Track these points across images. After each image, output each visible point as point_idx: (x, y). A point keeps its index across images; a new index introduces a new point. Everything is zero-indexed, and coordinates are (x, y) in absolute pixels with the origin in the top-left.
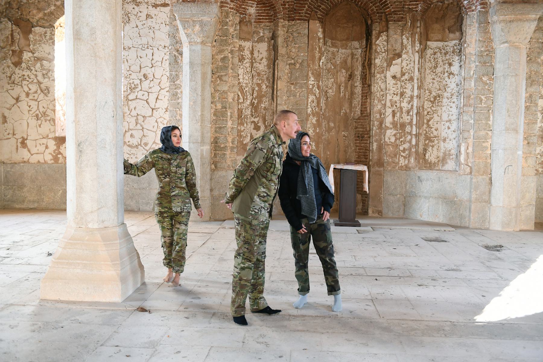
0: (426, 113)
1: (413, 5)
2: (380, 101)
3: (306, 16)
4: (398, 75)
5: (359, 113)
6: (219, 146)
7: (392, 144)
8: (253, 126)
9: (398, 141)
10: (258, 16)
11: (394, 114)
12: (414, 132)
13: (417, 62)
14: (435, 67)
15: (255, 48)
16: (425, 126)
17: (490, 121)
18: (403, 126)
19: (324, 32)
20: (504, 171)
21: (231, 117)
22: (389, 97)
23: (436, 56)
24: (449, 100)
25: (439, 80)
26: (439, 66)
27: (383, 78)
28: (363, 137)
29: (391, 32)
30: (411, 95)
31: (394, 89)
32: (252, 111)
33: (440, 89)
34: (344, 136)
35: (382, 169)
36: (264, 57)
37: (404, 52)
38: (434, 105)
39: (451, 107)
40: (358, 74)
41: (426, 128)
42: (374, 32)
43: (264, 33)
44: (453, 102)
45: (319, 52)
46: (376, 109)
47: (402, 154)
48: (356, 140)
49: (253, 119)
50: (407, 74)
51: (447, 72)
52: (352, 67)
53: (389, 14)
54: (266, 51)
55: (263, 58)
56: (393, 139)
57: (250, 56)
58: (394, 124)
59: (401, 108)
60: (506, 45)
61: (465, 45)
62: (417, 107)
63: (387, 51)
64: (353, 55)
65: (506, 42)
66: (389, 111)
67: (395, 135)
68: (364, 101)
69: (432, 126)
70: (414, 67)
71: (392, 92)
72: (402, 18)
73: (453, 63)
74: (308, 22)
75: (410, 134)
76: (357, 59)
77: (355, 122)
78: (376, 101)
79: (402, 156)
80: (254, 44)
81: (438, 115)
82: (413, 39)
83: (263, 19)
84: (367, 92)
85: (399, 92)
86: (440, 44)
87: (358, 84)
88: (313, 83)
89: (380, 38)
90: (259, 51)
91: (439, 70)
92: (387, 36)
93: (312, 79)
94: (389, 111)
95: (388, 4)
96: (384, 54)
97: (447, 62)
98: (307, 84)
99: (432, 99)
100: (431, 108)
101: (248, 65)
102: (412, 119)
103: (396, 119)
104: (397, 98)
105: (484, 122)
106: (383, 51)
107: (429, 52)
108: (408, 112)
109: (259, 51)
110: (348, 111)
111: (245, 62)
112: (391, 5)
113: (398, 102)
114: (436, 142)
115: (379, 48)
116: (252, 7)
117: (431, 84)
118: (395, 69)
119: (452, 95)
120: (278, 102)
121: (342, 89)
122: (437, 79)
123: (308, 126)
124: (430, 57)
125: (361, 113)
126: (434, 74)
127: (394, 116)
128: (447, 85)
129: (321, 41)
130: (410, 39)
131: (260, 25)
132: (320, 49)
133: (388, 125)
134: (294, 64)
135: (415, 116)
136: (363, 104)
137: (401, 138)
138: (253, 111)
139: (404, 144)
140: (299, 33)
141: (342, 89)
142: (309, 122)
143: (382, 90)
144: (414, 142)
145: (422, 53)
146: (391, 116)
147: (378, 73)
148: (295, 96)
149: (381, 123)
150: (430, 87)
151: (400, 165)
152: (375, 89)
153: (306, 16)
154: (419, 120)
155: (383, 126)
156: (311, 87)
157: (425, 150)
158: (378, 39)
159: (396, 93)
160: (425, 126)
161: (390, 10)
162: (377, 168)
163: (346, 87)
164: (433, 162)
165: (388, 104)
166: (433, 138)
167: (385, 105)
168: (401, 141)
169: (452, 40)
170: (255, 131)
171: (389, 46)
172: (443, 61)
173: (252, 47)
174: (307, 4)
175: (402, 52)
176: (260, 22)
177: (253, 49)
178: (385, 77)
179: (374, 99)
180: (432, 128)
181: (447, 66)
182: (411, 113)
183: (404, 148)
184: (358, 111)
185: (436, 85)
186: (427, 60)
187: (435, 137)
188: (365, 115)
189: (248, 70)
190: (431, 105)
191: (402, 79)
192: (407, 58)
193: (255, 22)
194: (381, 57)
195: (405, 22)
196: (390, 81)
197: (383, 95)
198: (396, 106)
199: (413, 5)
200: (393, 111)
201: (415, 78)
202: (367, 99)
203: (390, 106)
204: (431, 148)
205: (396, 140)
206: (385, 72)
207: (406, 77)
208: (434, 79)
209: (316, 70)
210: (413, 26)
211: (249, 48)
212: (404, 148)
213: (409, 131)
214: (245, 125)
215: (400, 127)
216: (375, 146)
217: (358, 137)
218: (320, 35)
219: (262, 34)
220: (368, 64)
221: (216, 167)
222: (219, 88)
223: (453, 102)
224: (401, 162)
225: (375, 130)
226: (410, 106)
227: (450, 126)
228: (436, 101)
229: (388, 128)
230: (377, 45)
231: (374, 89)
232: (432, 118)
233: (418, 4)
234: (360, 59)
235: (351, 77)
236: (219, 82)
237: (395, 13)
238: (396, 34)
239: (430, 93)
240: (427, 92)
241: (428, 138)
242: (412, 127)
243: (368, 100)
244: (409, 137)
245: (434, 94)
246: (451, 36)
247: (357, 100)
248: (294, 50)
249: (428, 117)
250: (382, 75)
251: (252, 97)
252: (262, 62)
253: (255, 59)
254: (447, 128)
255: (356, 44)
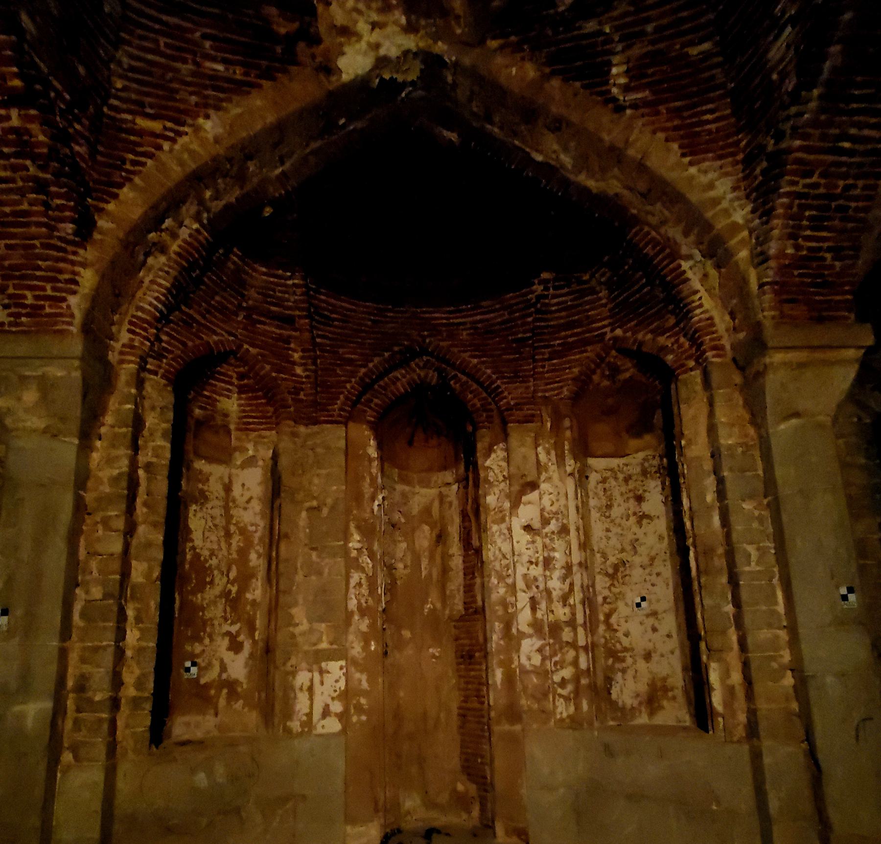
0: (600, 599)
1: (553, 389)
2: (501, 578)
3: (340, 416)
4: (536, 524)
5: (460, 607)
6: (90, 701)
7: (536, 671)
8: (226, 642)
9: (548, 662)
10: (245, 417)
11: (534, 604)
12: (582, 642)
13: (571, 494)
14: (609, 507)
15: (234, 480)
16: (602, 628)
17: (776, 603)
18: (555, 629)
19: (380, 447)
20: (853, 733)
21: (138, 620)
22: (521, 570)
23: (607, 485)
24: (647, 571)
25: (621, 532)
26: (615, 505)
27: (506, 531)
28: (471, 657)
29: (514, 441)
30: (567, 563)
31: (530, 552)
32: (225, 611)
33: (623, 550)
34: (434, 656)
35: (518, 728)
36: (255, 496)
37: (543, 478)
38: (616, 583)
39: (653, 585)
40: (454, 530)
41: (605, 631)
42: (479, 446)
43: (256, 450)
44: (658, 574)
45: (371, 485)
46: (494, 597)
47: (560, 691)
48: (460, 664)
49: (226, 628)
50: (553, 522)
51: (635, 514)
52: (442, 517)
53: (507, 410)
54: (260, 484)
55: (251, 498)
56: (537, 660)
57: (223, 494)
58: (537, 626)
59: (548, 592)
60: (794, 421)
61: (683, 442)
62: (582, 587)
63: (508, 478)
64: (442, 497)
65: (797, 415)
66: (523, 599)
67: (540, 650)
68: (468, 582)
69: (616, 627)
70: (566, 507)
71: (525, 559)
72: (533, 416)
73: (647, 494)
74: (346, 427)
75: (574, 645)
76: (451, 504)
77: (455, 627)
78: (494, 581)
79: (560, 696)
80: (234, 471)
81: (626, 604)
82: (559, 452)
83: (254, 423)
84: (474, 553)
85: (541, 558)
86: (615, 462)
87: (455, 549)
88: (358, 546)
89: (493, 456)
90: (243, 485)
91: (616, 512)
92: (507, 450)
93: (357, 537)
94: (523, 599)
95: (502, 392)
96: (503, 484)
97: (631, 494)
98: (346, 551)
99: (610, 571)
100: (609, 588)
101: (217, 512)
102: (574, 614)
103: (539, 615)
104: (536, 571)
105: (764, 608)
106: (501, 478)
107: (594, 478)
108: (564, 599)
109: (243, 485)
110: (439, 605)
111: (209, 505)
112: (509, 394)
113: (541, 579)
114: (629, 661)
115: (491, 474)
116: (229, 397)
117: (604, 540)
118: (528, 513)
119: (652, 559)
120: (282, 587)
121: (424, 563)
122: (615, 530)
123: (351, 637)
124: (596, 488)
125: (466, 609)
126: (608, 520)
127: (534, 609)
128: (637, 540)
129: (375, 463)
130: (553, 453)
131: (247, 435)
132: (373, 480)
133: (525, 628)
134: (318, 509)
135: (579, 608)
136: (469, 589)
137: (555, 654)
138: (228, 609)
139: (562, 668)
140: (328, 448)
141: (424, 563)
142: (352, 629)
143: (504, 557)
144: (583, 663)
145: (582, 478)
146: (528, 611)
147: (494, 522)
148: (320, 573)
149: (508, 626)
150: (602, 546)
151: (558, 717)
152: (490, 554)
153: (340, 416)
154: (590, 615)
155: (514, 631)
156: (354, 554)
157: (609, 680)
158: (489, 456)
159: (534, 560)
160: (602, 628)
161: (508, 403)
162: (507, 727)
163: (432, 558)
164: (628, 706)
165: (521, 584)
166: (622, 652)
167: (514, 585)
168: (556, 663)
169: (637, 451)
170: (231, 654)
171: (511, 468)
172: (622, 494)
173: (229, 478)
174: (342, 393)
175: (539, 478)
176: (247, 429)
177: (230, 482)
178: (510, 529)
179: (490, 576)
180: (616, 631)
181: (632, 503)
182: (571, 601)
183: (563, 678)
184: (459, 606)
185: (614, 541)
186: (591, 494)
187: (626, 649)
188: (475, 612)
189: (217, 521)
190: (608, 585)
191: (545, 531)
192: (551, 491)
193: (238, 429)
194: (497, 492)
195: (539, 424)
196: (521, 538)
197: (507, 567)
198: (537, 587)
199: (553, 389)
200: (532, 599)
201: (572, 529)
202: (474, 578)
203: (524, 588)
204: (620, 674)
205: (544, 659)
206: (507, 518)
207: (553, 526)
208: (608, 530)
209: (365, 521)
210: (557, 428)
211: (221, 478)
212: (563, 678)
213: (570, 640)
214: (207, 641)
215: (550, 631)
216: (498, 676)
217: (462, 657)
218: (373, 452)
219: (251, 453)
220: (473, 515)
221: (76, 757)
222: (99, 548)
223: (658, 574)
224: (559, 710)
225: (496, 639)
226: (566, 587)
227: (657, 625)
228: (619, 574)
229: (522, 635)
230: (488, 468)
231: (490, 553)
232: (615, 610)
233: (561, 387)
234: (455, 503)
235: (441, 538)
236: (100, 532)
237: (518, 406)
238: (523, 445)
239: (604, 556)
240: (598, 555)
241: (612, 653)
242: (575, 629)
243: (478, 581)
244: (571, 654)
245: (612, 560)
246: (633, 443)
247: (457, 582)
248: (316, 481)
249: (606, 608)
250: (503, 526)
251: (225, 579)
252: (250, 505)
253: (234, 501)
254: (649, 629)
255: (448, 476)
